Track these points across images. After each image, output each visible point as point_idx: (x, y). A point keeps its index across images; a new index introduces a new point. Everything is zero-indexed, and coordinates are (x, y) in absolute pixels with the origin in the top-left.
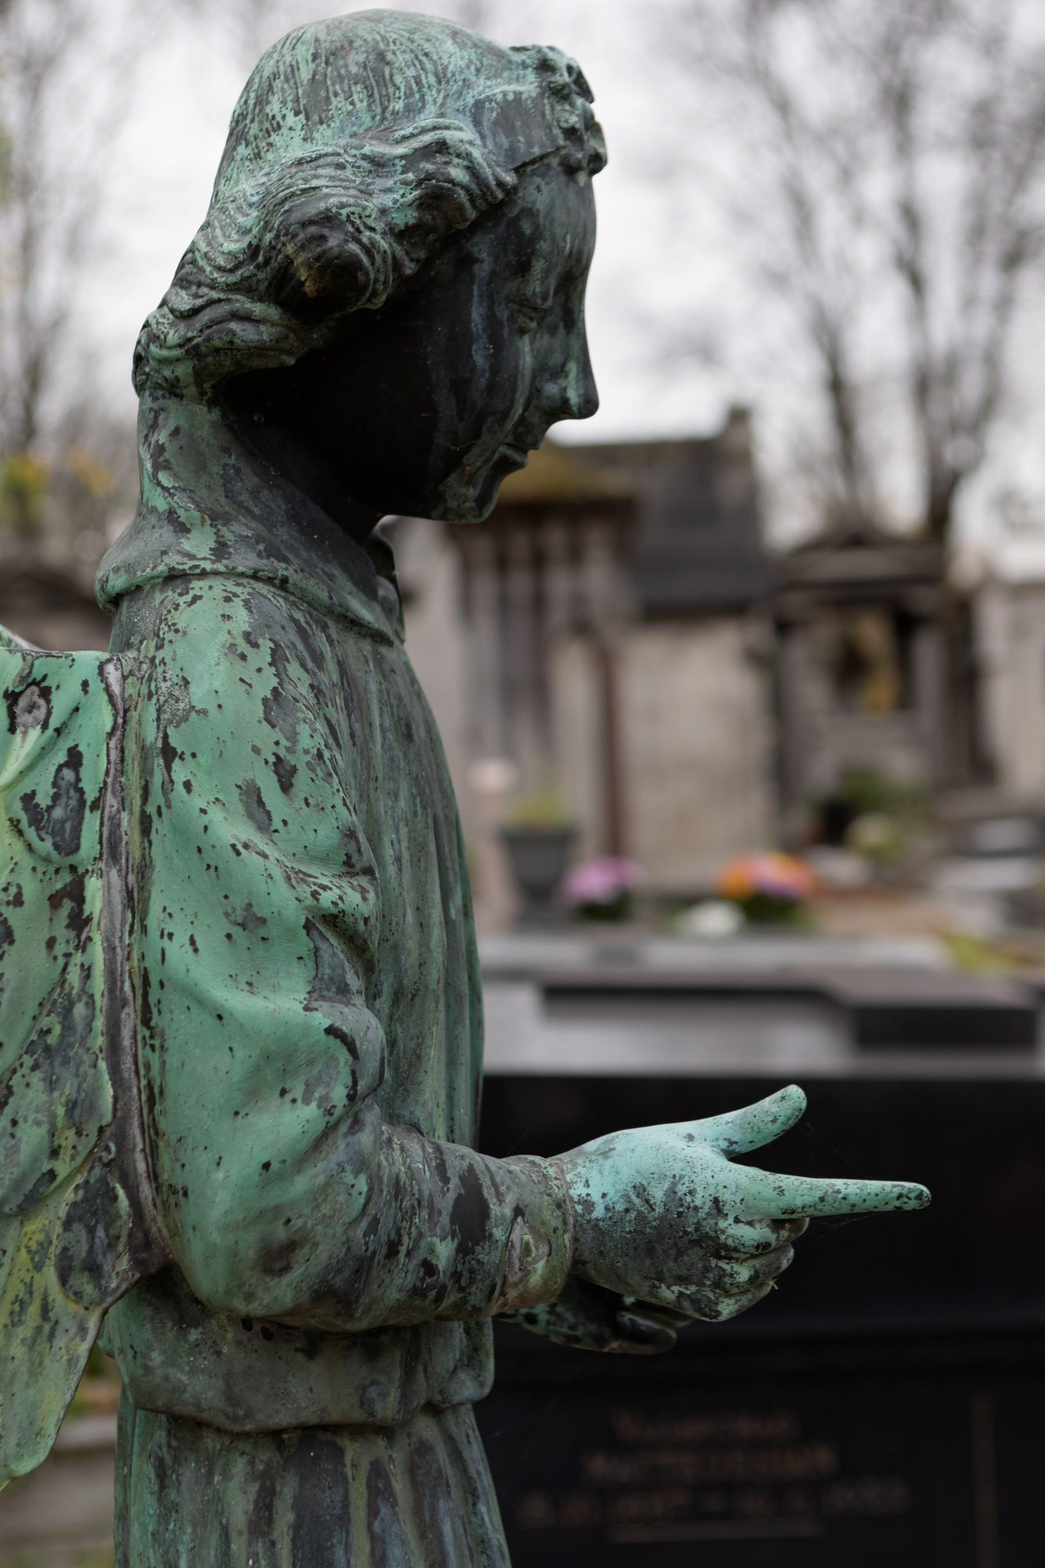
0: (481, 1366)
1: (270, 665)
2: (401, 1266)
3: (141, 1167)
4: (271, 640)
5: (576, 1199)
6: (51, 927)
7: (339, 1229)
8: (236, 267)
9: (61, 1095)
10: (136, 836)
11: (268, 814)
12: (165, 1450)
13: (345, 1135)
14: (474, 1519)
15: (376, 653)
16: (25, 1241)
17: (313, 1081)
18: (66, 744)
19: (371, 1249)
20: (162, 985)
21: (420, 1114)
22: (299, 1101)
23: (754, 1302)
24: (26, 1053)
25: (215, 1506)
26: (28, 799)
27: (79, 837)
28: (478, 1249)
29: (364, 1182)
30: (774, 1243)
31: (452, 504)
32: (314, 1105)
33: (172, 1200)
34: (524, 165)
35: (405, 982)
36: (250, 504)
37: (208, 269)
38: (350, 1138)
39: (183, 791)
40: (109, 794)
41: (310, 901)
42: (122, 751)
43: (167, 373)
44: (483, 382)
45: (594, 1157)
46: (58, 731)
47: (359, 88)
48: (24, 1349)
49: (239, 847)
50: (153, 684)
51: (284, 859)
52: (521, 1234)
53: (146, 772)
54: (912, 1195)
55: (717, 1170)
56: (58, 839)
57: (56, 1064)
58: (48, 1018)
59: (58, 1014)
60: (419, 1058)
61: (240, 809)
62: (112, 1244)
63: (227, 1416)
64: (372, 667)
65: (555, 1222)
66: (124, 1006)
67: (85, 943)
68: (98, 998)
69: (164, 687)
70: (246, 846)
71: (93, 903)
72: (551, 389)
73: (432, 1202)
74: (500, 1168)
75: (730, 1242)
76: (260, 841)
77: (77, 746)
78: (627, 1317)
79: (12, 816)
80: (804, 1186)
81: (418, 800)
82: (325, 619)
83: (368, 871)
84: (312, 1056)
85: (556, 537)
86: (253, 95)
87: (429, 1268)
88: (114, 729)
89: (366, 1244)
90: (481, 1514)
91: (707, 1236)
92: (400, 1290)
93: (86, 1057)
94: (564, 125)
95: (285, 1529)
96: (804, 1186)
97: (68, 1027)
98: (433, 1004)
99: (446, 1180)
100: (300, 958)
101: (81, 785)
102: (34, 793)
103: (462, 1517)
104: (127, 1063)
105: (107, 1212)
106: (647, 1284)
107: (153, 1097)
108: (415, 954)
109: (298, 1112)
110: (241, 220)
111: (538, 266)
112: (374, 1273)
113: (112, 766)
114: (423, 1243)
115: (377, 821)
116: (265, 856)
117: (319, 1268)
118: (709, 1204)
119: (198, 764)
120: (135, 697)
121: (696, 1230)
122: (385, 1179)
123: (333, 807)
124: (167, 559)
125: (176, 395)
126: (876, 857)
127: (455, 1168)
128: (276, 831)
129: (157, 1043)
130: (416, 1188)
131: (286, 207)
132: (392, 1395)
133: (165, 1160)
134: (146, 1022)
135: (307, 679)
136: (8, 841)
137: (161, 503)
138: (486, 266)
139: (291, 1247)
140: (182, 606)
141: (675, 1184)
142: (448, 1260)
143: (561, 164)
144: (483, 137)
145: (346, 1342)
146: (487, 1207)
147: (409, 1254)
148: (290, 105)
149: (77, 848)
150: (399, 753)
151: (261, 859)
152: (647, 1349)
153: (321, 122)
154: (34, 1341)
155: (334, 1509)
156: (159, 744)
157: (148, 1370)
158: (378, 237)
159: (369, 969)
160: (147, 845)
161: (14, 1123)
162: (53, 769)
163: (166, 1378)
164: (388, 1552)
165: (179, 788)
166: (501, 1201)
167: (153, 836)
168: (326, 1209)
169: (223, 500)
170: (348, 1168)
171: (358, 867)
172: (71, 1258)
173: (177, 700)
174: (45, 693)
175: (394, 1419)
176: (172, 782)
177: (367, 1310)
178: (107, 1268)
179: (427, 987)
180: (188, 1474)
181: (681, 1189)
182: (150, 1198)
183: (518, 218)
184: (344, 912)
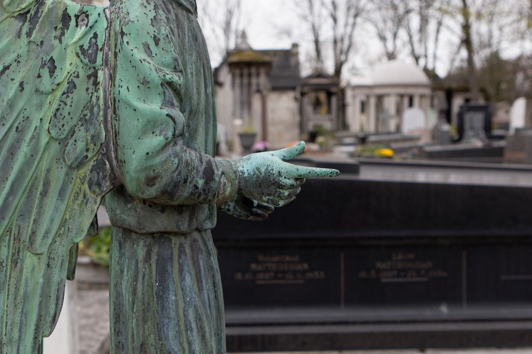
0: (213, 220)
1: (154, 9)
2: (188, 186)
3: (113, 155)
4: (154, 3)
5: (240, 171)
6: (87, 85)
7: (169, 174)
9: (90, 133)
10: (113, 58)
12: (121, 238)
13: (172, 147)
14: (209, 261)
15: (187, 15)
17: (162, 130)
18: (93, 32)
19: (179, 180)
20: (119, 101)
21: (196, 146)
22: (158, 135)
23: (289, 202)
24: (79, 121)
25: (134, 254)
26: (81, 47)
27: (96, 59)
28: (211, 183)
29: (177, 160)
30: (295, 185)
32: (162, 136)
35: (193, 108)
38: (173, 148)
39: (126, 44)
40: (105, 46)
41: (163, 77)
42: (110, 34)
45: (245, 160)
46: (91, 27)
49: (142, 60)
50: (119, 14)
51: (155, 65)
53: (116, 40)
54: (335, 173)
55: (280, 163)
56: (90, 59)
57: (88, 124)
58: (86, 111)
59: (89, 110)
60: (196, 130)
61: (143, 50)
62: (104, 178)
64: (186, 18)
65: (233, 177)
66: (108, 108)
67: (98, 90)
68: (101, 106)
69: (122, 15)
70: (144, 60)
71: (100, 78)
73: (198, 169)
74: (218, 161)
77: (96, 32)
78: (254, 210)
79: (77, 52)
80: (304, 169)
81: (198, 58)
82: (172, 2)
83: (181, 71)
84: (162, 122)
85: (253, 70)
87: (196, 187)
88: (107, 27)
89: (177, 178)
90: (211, 260)
91: (276, 182)
92: (188, 193)
93: (97, 123)
95: (154, 261)
96: (304, 169)
98: (201, 116)
99: (202, 163)
100: (159, 94)
101: (97, 43)
102: (83, 45)
103: (206, 260)
104: (109, 125)
105: (103, 168)
106: (259, 196)
107: (116, 134)
108: (196, 101)
109: (157, 138)
112: (180, 187)
113: (107, 38)
114: (194, 180)
115: (186, 61)
116: (150, 63)
117: (163, 185)
118: (277, 173)
119: (131, 37)
120: (114, 18)
121: (273, 180)
122: (184, 160)
123: (171, 51)
126: (321, 145)
127: (205, 160)
128: (153, 57)
129: (117, 118)
130: (193, 164)
132: (186, 224)
133: (119, 153)
134: (115, 113)
135: (165, 15)
139: (155, 178)
141: (268, 167)
142: (202, 185)
145: (173, 209)
146: (214, 171)
147: (190, 183)
149: (96, 62)
150: (193, 44)
151: (148, 64)
152: (260, 219)
155: (168, 255)
156: (120, 31)
157: (116, 215)
159: (181, 101)
160: (116, 61)
161: (76, 141)
162: (89, 39)
163: (121, 217)
164: (184, 268)
165: (125, 43)
166: (218, 170)
167: (118, 58)
168: (165, 167)
170: (172, 156)
171: (178, 70)
174: (87, 16)
175: (186, 231)
176: (123, 42)
177: (178, 198)
178: (103, 184)
179: (199, 111)
180: (127, 245)
181: (270, 169)
182: (116, 165)
184: (173, 81)
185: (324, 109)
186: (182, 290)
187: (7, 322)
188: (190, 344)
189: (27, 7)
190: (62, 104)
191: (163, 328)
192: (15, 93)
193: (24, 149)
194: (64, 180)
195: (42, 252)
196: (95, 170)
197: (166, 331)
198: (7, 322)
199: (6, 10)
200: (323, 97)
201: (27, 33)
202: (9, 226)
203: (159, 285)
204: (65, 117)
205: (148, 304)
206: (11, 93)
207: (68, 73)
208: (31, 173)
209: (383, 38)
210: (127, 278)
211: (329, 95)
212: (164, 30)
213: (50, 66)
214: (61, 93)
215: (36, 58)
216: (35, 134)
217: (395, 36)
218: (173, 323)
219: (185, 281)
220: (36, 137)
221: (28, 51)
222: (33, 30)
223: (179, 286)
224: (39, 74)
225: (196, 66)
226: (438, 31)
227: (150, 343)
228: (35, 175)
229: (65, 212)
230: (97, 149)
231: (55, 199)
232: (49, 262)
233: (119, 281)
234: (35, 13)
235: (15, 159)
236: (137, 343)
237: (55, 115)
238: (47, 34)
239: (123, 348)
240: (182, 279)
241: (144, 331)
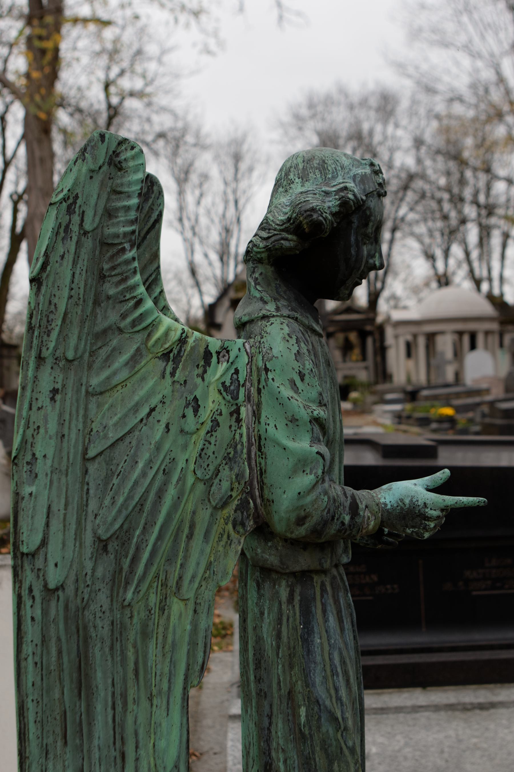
1: (296, 343)
3: (257, 493)
7: (319, 512)
8: (283, 224)
10: (256, 395)
11: (298, 388)
12: (259, 578)
13: (321, 484)
15: (319, 340)
16: (223, 516)
20: (266, 439)
26: (223, 383)
27: (238, 395)
31: (341, 295)
33: (268, 503)
34: (368, 194)
36: (284, 295)
37: (273, 225)
38: (322, 485)
39: (272, 381)
40: (247, 382)
41: (311, 414)
42: (251, 369)
43: (259, 256)
44: (354, 259)
46: (232, 363)
47: (317, 171)
48: (223, 548)
49: (290, 398)
50: (260, 349)
52: (367, 514)
57: (232, 463)
61: (289, 386)
62: (248, 517)
63: (281, 568)
65: (377, 510)
66: (252, 446)
68: (244, 443)
69: (264, 350)
72: (371, 261)
75: (429, 515)
76: (295, 396)
86: (283, 173)
87: (343, 523)
88: (248, 362)
91: (422, 514)
94: (378, 182)
97: (236, 452)
99: (347, 497)
102: (225, 382)
104: (253, 463)
107: (262, 473)
108: (332, 430)
110: (284, 210)
111: (371, 224)
114: (342, 516)
116: (298, 401)
118: (423, 504)
121: (419, 512)
124: (262, 312)
125: (261, 263)
126: (355, 402)
129: (264, 457)
131: (300, 206)
133: (266, 492)
134: (260, 449)
136: (217, 396)
137: (258, 295)
138: (356, 224)
139: (305, 517)
140: (268, 326)
141: (412, 498)
143: (377, 194)
144: (356, 186)
147: (337, 519)
148: (296, 176)
149: (238, 398)
153: (307, 181)
154: (225, 546)
156: (264, 367)
157: (257, 554)
158: (328, 215)
161: (220, 481)
162: (230, 375)
163: (262, 557)
165: (270, 380)
166: (362, 504)
167: (262, 394)
168: (316, 506)
169: (276, 294)
170: (322, 494)
171: (323, 404)
172: (237, 521)
173: (269, 354)
174: (228, 352)
176: (268, 378)
178: (247, 524)
181: (414, 500)
183: (366, 210)
185: (356, 352)
186: (327, 631)
187: (156, 673)
188: (336, 690)
189: (170, 346)
190: (207, 443)
191: (310, 674)
192: (162, 435)
193: (171, 492)
194: (209, 522)
195: (188, 597)
196: (239, 510)
197: (313, 676)
198: (156, 673)
199: (151, 351)
200: (353, 337)
201: (170, 373)
202: (157, 572)
203: (304, 628)
204: (209, 456)
205: (294, 648)
206: (158, 436)
207: (211, 411)
208: (177, 516)
209: (430, 257)
210: (268, 621)
211: (363, 335)
212: (309, 365)
213: (194, 405)
214: (206, 432)
215: (181, 398)
216: (181, 476)
217: (447, 253)
218: (319, 668)
219: (329, 621)
220: (182, 479)
221: (173, 391)
222: (176, 370)
223: (323, 627)
224: (184, 414)
225: (331, 393)
226: (504, 246)
227: (298, 690)
228: (181, 518)
229: (210, 554)
230: (241, 488)
231: (201, 542)
232: (195, 608)
233: (258, 624)
234: (178, 352)
235: (163, 502)
236: (285, 691)
237: (200, 455)
238: (190, 372)
239: (266, 697)
240: (326, 620)
241: (291, 677)
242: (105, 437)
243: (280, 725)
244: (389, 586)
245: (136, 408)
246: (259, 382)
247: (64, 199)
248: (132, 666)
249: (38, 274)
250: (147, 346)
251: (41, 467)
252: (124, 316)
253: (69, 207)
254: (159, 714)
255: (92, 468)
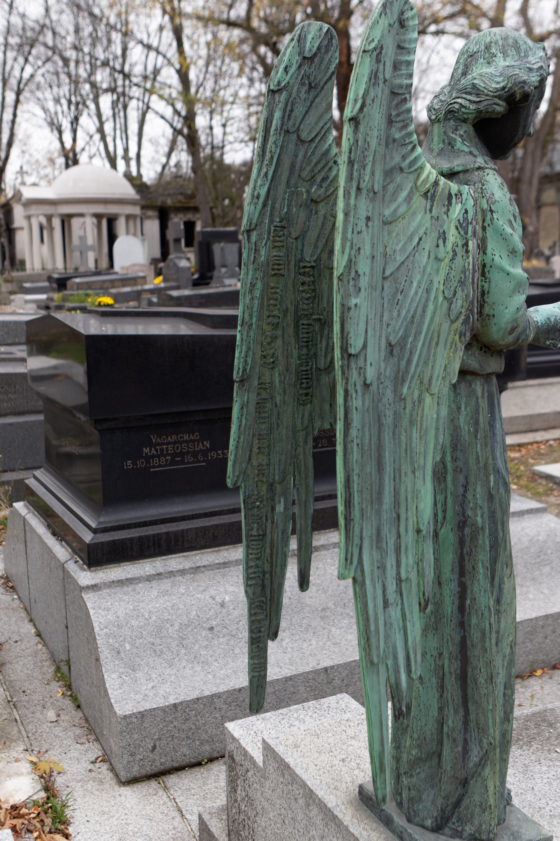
26: (459, 220)
43: (465, 116)
69: (488, 195)
97: (465, 277)
174: (461, 195)
193: (431, 307)
198: (406, 454)
220: (436, 298)
239: (461, 472)
242: (395, 260)
243: (479, 489)
244: (220, 452)
245: (411, 238)
246: (484, 221)
247: (375, 49)
248: (404, 446)
249: (358, 113)
250: (416, 185)
251: (364, 282)
252: (404, 158)
253: (377, 56)
254: (419, 482)
255: (387, 284)
